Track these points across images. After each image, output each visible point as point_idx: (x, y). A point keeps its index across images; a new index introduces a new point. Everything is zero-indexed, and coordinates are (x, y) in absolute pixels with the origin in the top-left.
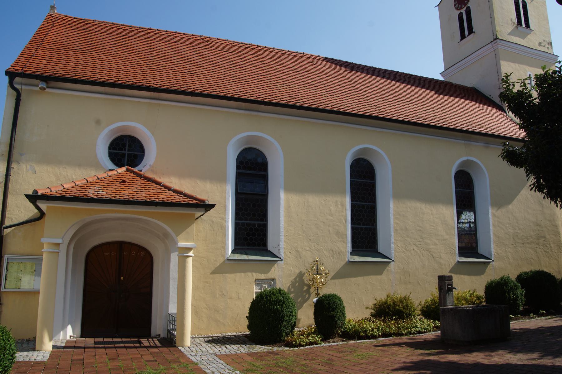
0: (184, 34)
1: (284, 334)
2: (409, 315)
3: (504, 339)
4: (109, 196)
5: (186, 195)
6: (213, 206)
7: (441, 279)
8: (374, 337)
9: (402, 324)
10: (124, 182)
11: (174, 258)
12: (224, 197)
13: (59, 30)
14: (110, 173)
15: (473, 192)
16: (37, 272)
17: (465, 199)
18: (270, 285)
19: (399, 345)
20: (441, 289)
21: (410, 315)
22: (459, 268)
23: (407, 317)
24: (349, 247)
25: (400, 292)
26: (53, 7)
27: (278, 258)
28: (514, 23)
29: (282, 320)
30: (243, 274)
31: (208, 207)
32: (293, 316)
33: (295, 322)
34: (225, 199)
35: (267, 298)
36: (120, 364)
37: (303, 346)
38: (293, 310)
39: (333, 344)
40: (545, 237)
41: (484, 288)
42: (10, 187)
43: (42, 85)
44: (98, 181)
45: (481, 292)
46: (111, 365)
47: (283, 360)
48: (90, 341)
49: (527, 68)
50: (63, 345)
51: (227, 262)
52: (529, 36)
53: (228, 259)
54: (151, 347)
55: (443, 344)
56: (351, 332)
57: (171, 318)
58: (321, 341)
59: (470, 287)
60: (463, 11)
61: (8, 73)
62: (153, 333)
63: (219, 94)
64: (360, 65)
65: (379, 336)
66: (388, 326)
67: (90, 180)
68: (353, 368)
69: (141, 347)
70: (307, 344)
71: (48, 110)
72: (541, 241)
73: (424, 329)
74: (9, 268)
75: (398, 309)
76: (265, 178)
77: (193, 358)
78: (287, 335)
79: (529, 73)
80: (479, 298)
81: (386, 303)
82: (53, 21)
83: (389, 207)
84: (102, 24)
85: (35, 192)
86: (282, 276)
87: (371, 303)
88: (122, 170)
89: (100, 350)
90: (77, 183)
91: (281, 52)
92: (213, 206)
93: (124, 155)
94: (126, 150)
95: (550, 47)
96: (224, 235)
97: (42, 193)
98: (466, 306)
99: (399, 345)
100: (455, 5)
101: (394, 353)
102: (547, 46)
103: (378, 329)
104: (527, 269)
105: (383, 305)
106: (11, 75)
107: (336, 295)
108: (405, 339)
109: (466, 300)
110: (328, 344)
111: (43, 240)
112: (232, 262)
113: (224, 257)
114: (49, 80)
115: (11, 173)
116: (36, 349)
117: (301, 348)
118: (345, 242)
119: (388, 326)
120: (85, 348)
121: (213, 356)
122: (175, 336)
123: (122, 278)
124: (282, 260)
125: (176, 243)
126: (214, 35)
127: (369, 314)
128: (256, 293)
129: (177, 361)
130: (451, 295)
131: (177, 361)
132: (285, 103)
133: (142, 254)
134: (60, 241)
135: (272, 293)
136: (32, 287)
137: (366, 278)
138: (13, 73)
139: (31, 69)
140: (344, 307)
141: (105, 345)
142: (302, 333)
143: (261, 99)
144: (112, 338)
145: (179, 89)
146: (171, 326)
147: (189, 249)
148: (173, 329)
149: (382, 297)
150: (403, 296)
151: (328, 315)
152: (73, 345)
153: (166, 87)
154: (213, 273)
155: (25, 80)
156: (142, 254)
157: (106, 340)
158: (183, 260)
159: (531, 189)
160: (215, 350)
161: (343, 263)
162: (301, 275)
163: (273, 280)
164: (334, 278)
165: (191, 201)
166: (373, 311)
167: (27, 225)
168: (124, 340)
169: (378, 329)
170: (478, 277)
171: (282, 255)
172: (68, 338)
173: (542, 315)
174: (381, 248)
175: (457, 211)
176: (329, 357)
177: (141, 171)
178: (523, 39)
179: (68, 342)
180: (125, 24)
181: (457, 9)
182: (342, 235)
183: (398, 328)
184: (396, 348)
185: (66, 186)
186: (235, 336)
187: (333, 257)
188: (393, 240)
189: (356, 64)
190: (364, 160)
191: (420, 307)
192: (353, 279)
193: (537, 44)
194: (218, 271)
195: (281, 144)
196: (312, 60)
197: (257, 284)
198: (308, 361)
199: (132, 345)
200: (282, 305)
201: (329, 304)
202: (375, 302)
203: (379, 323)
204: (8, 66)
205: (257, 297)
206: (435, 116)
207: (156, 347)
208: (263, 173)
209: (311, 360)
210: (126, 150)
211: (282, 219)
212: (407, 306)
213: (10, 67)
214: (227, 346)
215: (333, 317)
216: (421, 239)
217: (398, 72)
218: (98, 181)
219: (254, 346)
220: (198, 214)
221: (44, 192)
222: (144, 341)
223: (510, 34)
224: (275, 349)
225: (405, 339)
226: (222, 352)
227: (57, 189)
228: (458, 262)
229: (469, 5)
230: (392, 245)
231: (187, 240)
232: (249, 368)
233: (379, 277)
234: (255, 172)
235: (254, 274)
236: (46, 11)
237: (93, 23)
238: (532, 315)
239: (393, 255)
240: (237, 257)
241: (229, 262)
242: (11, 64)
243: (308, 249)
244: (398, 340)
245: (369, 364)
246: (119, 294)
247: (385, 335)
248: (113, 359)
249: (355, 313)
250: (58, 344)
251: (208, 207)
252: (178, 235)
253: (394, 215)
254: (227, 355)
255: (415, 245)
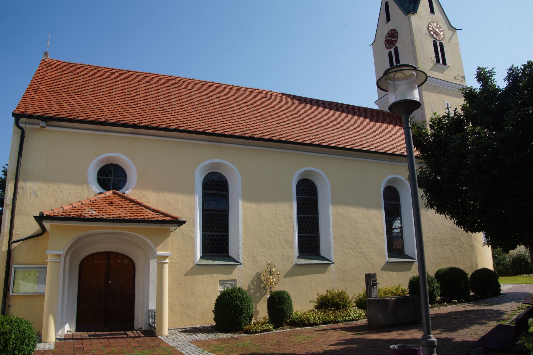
0: (157, 75)
1: (243, 324)
2: (345, 306)
3: (413, 322)
4: (101, 216)
5: (163, 214)
6: (184, 222)
7: (368, 276)
8: (315, 324)
9: (338, 313)
10: (112, 203)
11: (153, 264)
12: (190, 207)
13: (53, 74)
14: (100, 196)
15: (400, 204)
16: (42, 280)
17: (393, 211)
18: (232, 284)
19: (335, 329)
20: (367, 284)
21: (346, 306)
22: (388, 267)
23: (343, 308)
24: (297, 254)
25: (338, 288)
26: (46, 54)
27: (238, 262)
28: (433, 61)
29: (241, 313)
30: (209, 276)
31: (180, 223)
32: (250, 309)
33: (252, 314)
34: (194, 215)
35: (229, 295)
36: (114, 349)
37: (258, 333)
38: (250, 304)
39: (283, 331)
40: (459, 239)
41: (407, 283)
42: (17, 208)
43: (43, 124)
44: (91, 203)
45: (405, 286)
46: (106, 350)
47: (242, 343)
48: (85, 334)
49: (444, 97)
50: (63, 337)
51: (196, 267)
52: (446, 72)
53: (197, 265)
54: (136, 337)
55: (370, 328)
56: (297, 321)
57: (151, 314)
58: (274, 328)
59: (395, 282)
60: (392, 50)
61: (14, 115)
62: (136, 327)
63: (187, 129)
64: (305, 98)
65: (320, 324)
66: (327, 316)
67: (84, 202)
68: (296, 346)
69: (128, 337)
70: (262, 331)
71: (45, 143)
72: (457, 243)
73: (357, 317)
74: (16, 276)
75: (336, 302)
76: (226, 197)
77: (171, 344)
78: (246, 324)
79: (446, 102)
80: (403, 291)
81: (326, 297)
82: (48, 66)
83: (329, 219)
84: (88, 67)
85: (42, 213)
86: (242, 277)
87: (315, 297)
88: (109, 193)
89: (95, 341)
90: (74, 205)
91: (239, 89)
92: (184, 222)
93: (109, 180)
94: (111, 177)
95: (463, 80)
96: (194, 245)
97: (47, 215)
98: (390, 297)
99: (335, 329)
100: (385, 45)
101: (329, 336)
102: (461, 79)
103: (319, 318)
104: (444, 266)
105: (323, 298)
106: (17, 116)
107: (284, 292)
108: (341, 325)
109: (392, 293)
110: (279, 331)
111: (48, 252)
112: (200, 267)
113: (193, 262)
114: (48, 120)
115: (18, 197)
116: (43, 340)
117: (257, 334)
118: (293, 248)
119: (327, 316)
120: (81, 339)
121: (187, 342)
122: (155, 328)
123: (110, 282)
124: (241, 264)
125: (155, 252)
126: (183, 75)
127: (313, 306)
128: (220, 291)
129: (158, 346)
130: (375, 289)
131: (158, 346)
132: (242, 135)
133: (126, 261)
134: (61, 253)
135: (233, 291)
136: (35, 291)
137: (310, 275)
138: (19, 114)
139: (32, 111)
140: (291, 301)
141: (98, 337)
142: (258, 323)
143: (222, 133)
144: (102, 331)
145: (155, 125)
146: (151, 321)
147: (166, 257)
148: (154, 323)
149: (323, 292)
150: (340, 291)
151: (279, 307)
152: (71, 337)
153: (144, 124)
154: (186, 275)
155: (28, 120)
156: (126, 261)
157: (97, 333)
158: (160, 266)
159: (426, 207)
160: (188, 337)
161: (291, 266)
162: (258, 275)
163: (234, 280)
164: (285, 276)
165: (167, 219)
166: (316, 304)
167: (31, 240)
168: (112, 332)
169: (319, 318)
170: (401, 274)
171: (241, 260)
172: (66, 332)
173: (455, 303)
174: (323, 253)
175: (387, 221)
176: (278, 339)
177: (124, 193)
178: (442, 73)
179: (65, 335)
180: (108, 67)
181: (387, 48)
182: (290, 243)
183: (335, 317)
184: (332, 332)
185: (65, 208)
186: (204, 327)
187: (283, 261)
188: (332, 246)
189: (302, 98)
190: (308, 180)
191: (354, 300)
192: (300, 278)
193: (453, 78)
194: (190, 273)
195: (238, 167)
196: (266, 95)
197: (221, 285)
198: (261, 343)
199: (120, 336)
200: (241, 300)
201: (279, 299)
202: (318, 297)
203: (321, 314)
204: (14, 109)
205: (221, 295)
206: (367, 142)
207: (140, 337)
208: (224, 193)
209: (264, 342)
210: (111, 177)
211: (241, 230)
212: (343, 299)
213: (15, 109)
214: (197, 334)
215: (282, 309)
216: (357, 242)
217: (337, 103)
218: (91, 203)
219: (219, 334)
220: (172, 228)
221: (48, 213)
222: (129, 333)
223: (430, 70)
224: (236, 336)
225: (341, 325)
226: (194, 339)
227: (59, 211)
228: (387, 262)
229: (397, 45)
230: (332, 250)
231: (164, 250)
232: (216, 349)
233: (321, 275)
234: (218, 192)
235: (218, 275)
236: (42, 57)
237: (80, 67)
238: (446, 303)
239: (333, 257)
240: (205, 262)
241: (198, 267)
242: (16, 107)
243: (262, 254)
244: (335, 326)
245: (308, 343)
246: (107, 294)
247: (324, 323)
248: (107, 346)
249: (302, 305)
250: (59, 337)
251: (180, 223)
252: (156, 246)
253: (333, 225)
254: (197, 341)
255: (351, 249)
